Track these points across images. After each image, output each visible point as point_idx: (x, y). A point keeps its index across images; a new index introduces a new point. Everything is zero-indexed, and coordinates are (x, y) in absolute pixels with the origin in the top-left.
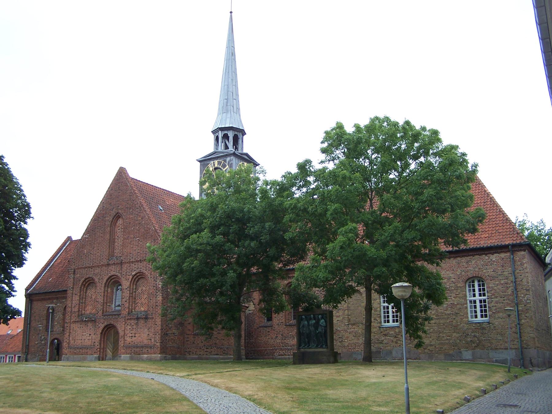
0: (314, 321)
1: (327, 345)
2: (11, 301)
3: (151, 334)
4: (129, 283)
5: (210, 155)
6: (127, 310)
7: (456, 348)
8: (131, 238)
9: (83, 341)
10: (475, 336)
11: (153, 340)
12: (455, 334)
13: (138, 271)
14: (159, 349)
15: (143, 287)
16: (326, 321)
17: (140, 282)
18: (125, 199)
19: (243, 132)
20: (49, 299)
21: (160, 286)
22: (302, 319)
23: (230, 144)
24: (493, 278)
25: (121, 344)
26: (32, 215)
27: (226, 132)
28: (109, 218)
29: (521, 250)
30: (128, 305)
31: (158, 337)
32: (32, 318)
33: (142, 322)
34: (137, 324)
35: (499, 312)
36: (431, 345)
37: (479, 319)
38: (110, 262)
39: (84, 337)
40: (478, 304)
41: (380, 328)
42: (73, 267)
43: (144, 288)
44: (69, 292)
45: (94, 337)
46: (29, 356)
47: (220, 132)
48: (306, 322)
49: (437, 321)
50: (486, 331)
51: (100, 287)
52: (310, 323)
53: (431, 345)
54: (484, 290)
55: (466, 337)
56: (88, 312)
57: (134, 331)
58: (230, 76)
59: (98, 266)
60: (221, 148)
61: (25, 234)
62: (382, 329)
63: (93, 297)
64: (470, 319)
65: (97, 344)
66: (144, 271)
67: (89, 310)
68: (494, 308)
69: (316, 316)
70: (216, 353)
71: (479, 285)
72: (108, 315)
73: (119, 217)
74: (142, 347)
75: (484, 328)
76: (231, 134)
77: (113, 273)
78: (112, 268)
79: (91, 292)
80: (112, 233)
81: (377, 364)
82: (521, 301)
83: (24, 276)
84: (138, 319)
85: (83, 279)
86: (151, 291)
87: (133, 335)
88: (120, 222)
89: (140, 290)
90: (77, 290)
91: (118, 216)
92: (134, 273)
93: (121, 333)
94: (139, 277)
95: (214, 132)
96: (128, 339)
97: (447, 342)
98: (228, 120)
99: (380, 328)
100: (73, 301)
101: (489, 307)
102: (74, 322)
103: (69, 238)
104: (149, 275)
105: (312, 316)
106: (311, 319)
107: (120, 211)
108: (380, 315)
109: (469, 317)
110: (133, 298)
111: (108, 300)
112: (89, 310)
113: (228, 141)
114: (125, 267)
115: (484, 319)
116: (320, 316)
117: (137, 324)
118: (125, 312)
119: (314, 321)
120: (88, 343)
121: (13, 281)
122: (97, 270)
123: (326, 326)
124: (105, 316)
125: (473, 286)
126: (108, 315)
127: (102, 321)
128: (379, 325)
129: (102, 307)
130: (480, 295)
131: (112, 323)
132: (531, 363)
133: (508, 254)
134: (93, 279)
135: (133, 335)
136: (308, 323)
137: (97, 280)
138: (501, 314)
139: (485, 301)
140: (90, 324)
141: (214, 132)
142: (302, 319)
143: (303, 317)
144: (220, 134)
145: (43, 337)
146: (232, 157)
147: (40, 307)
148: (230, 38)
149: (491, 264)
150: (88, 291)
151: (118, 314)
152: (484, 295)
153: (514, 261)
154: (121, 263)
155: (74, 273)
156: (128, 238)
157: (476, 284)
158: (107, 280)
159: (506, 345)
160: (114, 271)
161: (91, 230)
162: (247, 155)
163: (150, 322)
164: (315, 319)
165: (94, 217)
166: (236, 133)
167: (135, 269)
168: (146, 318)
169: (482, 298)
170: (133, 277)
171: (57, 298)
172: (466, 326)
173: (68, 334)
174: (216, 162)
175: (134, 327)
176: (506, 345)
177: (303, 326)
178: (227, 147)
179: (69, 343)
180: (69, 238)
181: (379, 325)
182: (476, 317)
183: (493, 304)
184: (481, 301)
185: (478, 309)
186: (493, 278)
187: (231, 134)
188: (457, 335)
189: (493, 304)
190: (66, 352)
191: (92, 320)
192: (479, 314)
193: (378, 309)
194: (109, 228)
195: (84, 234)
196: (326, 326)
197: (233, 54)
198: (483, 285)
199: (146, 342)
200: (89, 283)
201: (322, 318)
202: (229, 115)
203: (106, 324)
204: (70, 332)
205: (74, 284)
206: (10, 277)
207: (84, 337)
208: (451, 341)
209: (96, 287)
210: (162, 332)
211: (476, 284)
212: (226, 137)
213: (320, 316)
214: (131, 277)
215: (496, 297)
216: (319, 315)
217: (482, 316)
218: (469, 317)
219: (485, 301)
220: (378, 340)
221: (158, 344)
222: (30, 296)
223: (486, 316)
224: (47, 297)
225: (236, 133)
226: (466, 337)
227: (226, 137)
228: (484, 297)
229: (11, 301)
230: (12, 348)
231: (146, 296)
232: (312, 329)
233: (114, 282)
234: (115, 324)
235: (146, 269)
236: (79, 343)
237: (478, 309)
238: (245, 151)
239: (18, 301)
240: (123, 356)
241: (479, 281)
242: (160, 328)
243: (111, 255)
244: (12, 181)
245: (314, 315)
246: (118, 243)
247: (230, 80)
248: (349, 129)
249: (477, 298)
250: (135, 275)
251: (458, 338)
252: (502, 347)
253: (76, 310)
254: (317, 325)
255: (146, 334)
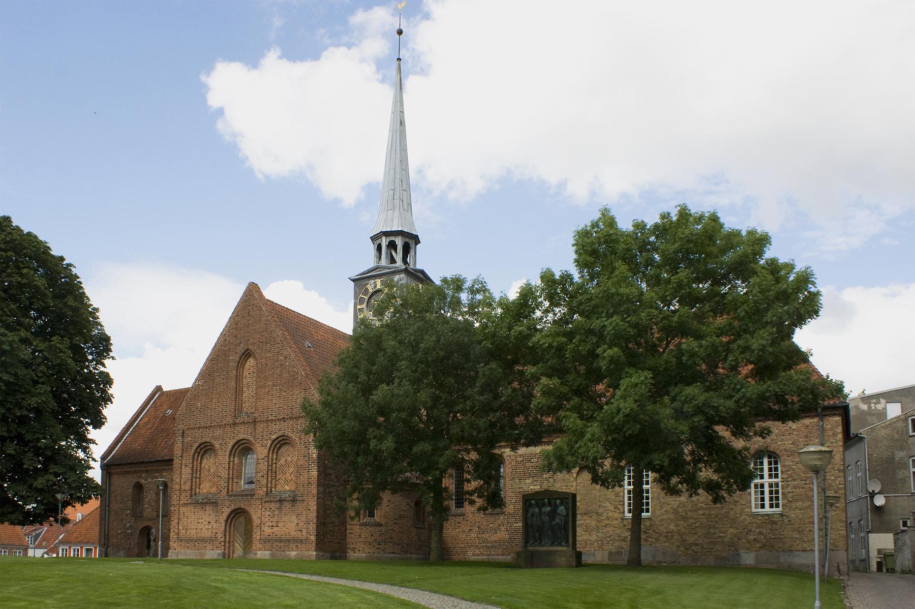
0: (549, 509)
1: (567, 542)
2: (90, 474)
3: (302, 524)
4: (266, 451)
5: (369, 271)
6: (265, 489)
7: (732, 549)
8: (268, 386)
9: (199, 531)
10: (760, 533)
11: (304, 531)
12: (731, 530)
13: (280, 433)
14: (314, 544)
15: (288, 456)
16: (567, 509)
17: (283, 449)
18: (256, 328)
19: (416, 239)
20: (135, 472)
21: (314, 456)
22: (531, 505)
23: (398, 257)
24: (791, 453)
25: (256, 535)
26: (111, 354)
27: (392, 238)
28: (234, 358)
29: (835, 415)
30: (265, 481)
31: (312, 527)
32: (112, 499)
33: (287, 505)
34: (280, 509)
35: (797, 501)
36: (696, 545)
37: (767, 509)
38: (237, 421)
39: (200, 526)
40: (767, 489)
41: (623, 519)
42: (181, 427)
43: (289, 459)
44: (176, 462)
45: (215, 525)
46: (110, 549)
47: (384, 238)
48: (537, 510)
49: (707, 512)
50: (777, 527)
51: (223, 457)
52: (544, 510)
53: (696, 545)
54: (776, 469)
55: (747, 533)
56: (205, 491)
57: (276, 519)
58: (398, 155)
59: (220, 426)
60: (384, 262)
61: (107, 380)
62: (625, 522)
63: (212, 470)
64: (754, 510)
65: (220, 535)
66: (290, 435)
67: (206, 488)
68: (791, 495)
69: (553, 501)
70: (391, 551)
71: (770, 463)
72: (236, 496)
73: (250, 356)
74: (289, 541)
75: (774, 523)
76: (399, 242)
77: (241, 436)
78: (241, 429)
79: (208, 463)
80: (238, 378)
81: (538, 567)
82: (830, 485)
83: (102, 439)
84: (281, 501)
85: (197, 444)
86: (301, 463)
87: (275, 524)
88: (251, 362)
89: (282, 461)
90: (188, 459)
91: (247, 354)
92: (274, 437)
93: (256, 522)
94: (281, 442)
95: (374, 239)
96: (267, 530)
97: (719, 540)
98: (396, 221)
99: (623, 519)
100: (181, 475)
101: (783, 494)
102: (186, 505)
103: (159, 388)
104: (297, 439)
105: (546, 500)
106: (544, 505)
107: (251, 347)
108: (623, 501)
109: (753, 506)
110: (272, 472)
111: (235, 474)
112: (206, 488)
113: (396, 251)
114: (260, 427)
115: (774, 509)
116: (533, 502)
117: (280, 509)
118: (262, 492)
119: (549, 509)
120: (207, 534)
121: (91, 446)
122: (218, 432)
123: (567, 516)
124: (231, 496)
125: (762, 463)
126: (236, 496)
127: (227, 503)
128: (621, 515)
129: (226, 485)
130: (770, 476)
131: (243, 506)
132: (839, 570)
133: (816, 420)
134: (212, 445)
135: (275, 524)
136: (540, 511)
137: (217, 445)
138: (801, 503)
139: (777, 485)
140: (208, 508)
141: (374, 239)
142: (531, 505)
143: (533, 502)
144: (384, 242)
145: (128, 525)
146: (403, 275)
147: (124, 484)
148: (398, 99)
149: (790, 434)
150: (204, 462)
151: (251, 495)
152: (776, 476)
153: (823, 430)
154: (255, 422)
155: (183, 436)
156: (264, 387)
157: (766, 461)
158: (233, 447)
159: (805, 545)
160: (243, 433)
161: (208, 373)
162: (422, 272)
163: (300, 507)
164: (550, 505)
165: (211, 355)
166: (407, 240)
167: (277, 430)
168: (294, 501)
169: (773, 480)
170: (273, 442)
171: (147, 471)
172: (749, 520)
173: (176, 521)
174: (378, 281)
175: (276, 513)
176: (805, 545)
177: (533, 515)
178: (393, 261)
179: (178, 534)
180: (159, 388)
181: (621, 515)
182: (763, 506)
183: (789, 490)
184: (771, 486)
185: (767, 496)
186: (791, 453)
187: (399, 242)
188: (735, 532)
189: (789, 490)
190: (175, 545)
191: (211, 502)
192: (767, 502)
193: (621, 494)
194: (234, 372)
195: (196, 380)
196: (567, 516)
197: (402, 123)
198: (776, 463)
199: (294, 534)
200: (205, 449)
201: (561, 504)
202: (397, 213)
203: (233, 507)
204: (179, 519)
205: (183, 450)
206: (84, 442)
207: (200, 526)
208: (726, 540)
209: (216, 455)
210: (317, 521)
211: (766, 461)
212: (392, 245)
213: (558, 502)
214: (270, 442)
215: (795, 480)
216: (556, 499)
217: (771, 506)
218: (753, 506)
219: (777, 485)
220: (620, 536)
221: (313, 538)
222: (107, 468)
223: (777, 506)
224: (133, 469)
225: (407, 240)
226: (747, 533)
227: (392, 245)
228: (776, 480)
229: (90, 474)
230: (76, 538)
231: (292, 469)
232: (546, 518)
233: (243, 448)
234: (246, 508)
235: (294, 430)
236: (193, 533)
237: (767, 496)
238: (419, 267)
239: (95, 474)
240: (259, 552)
241: (770, 457)
242: (315, 514)
243: (238, 411)
244: (82, 302)
245: (549, 500)
246: (248, 393)
247: (398, 162)
248: (625, 225)
249: (766, 480)
250: (276, 439)
251: (735, 535)
252: (800, 548)
253: (188, 487)
254: (553, 514)
255: (299, 523)
